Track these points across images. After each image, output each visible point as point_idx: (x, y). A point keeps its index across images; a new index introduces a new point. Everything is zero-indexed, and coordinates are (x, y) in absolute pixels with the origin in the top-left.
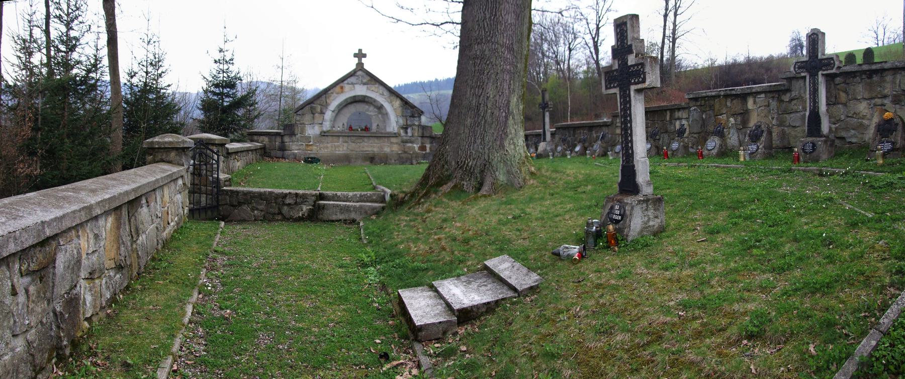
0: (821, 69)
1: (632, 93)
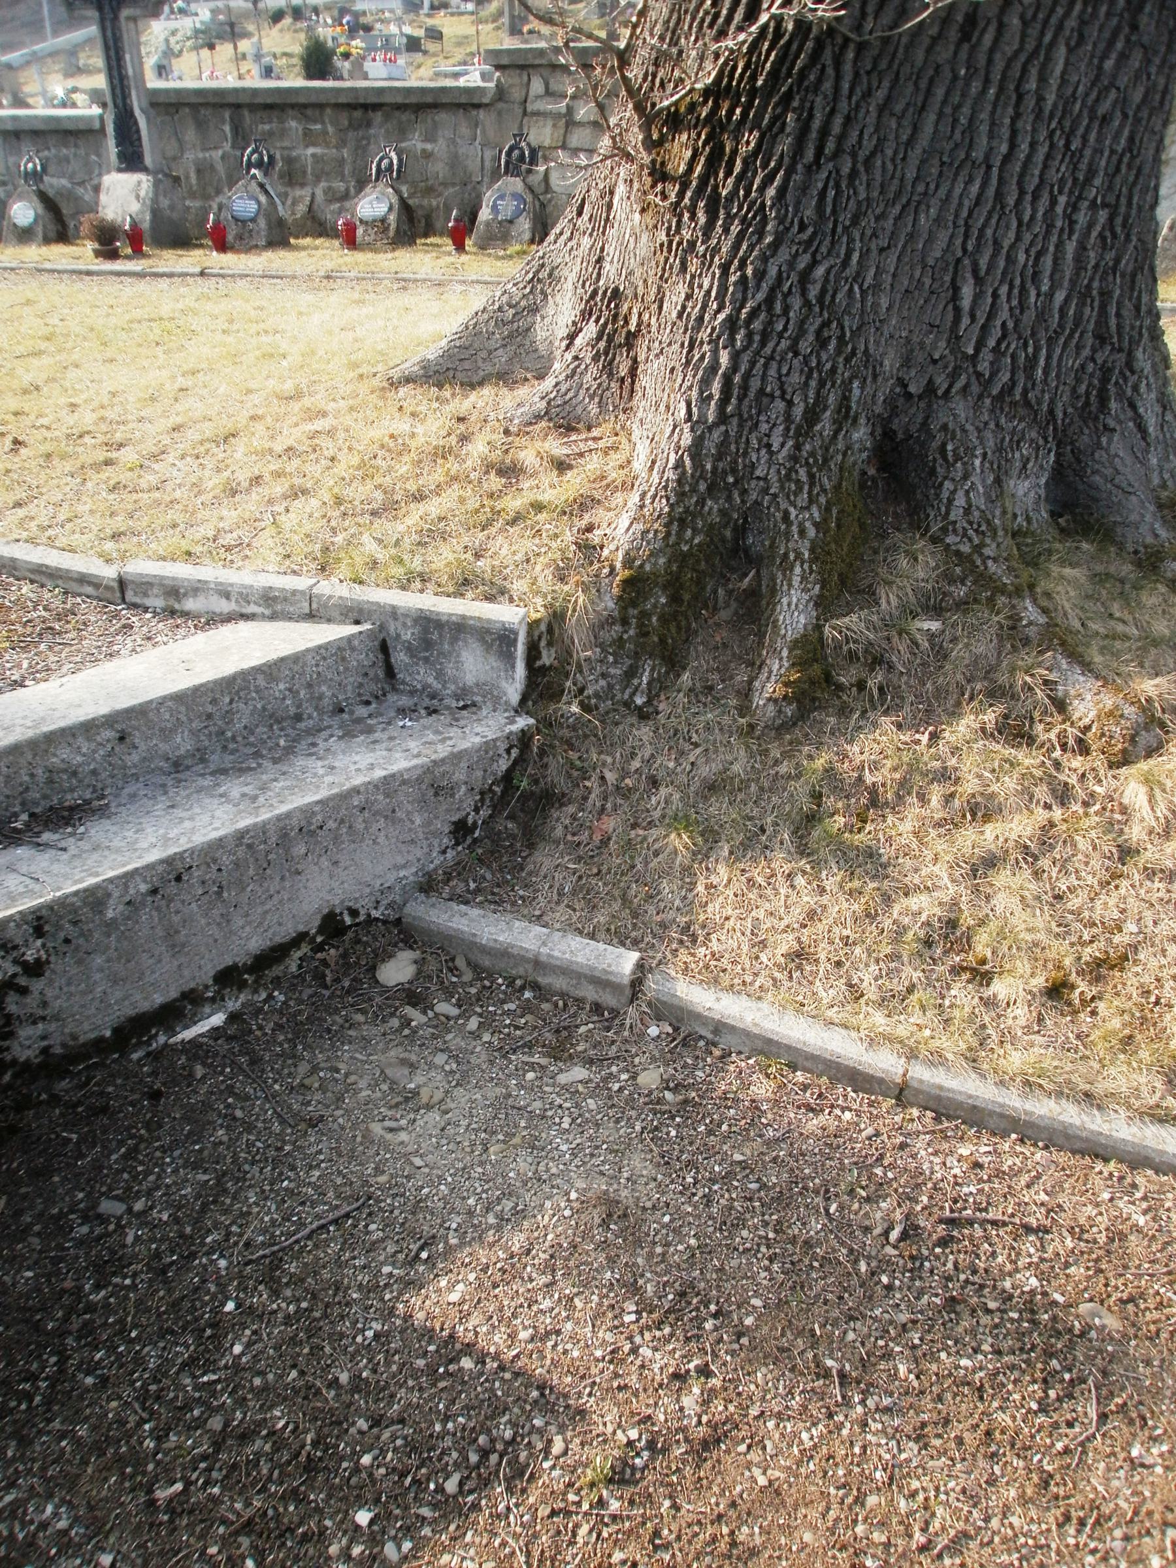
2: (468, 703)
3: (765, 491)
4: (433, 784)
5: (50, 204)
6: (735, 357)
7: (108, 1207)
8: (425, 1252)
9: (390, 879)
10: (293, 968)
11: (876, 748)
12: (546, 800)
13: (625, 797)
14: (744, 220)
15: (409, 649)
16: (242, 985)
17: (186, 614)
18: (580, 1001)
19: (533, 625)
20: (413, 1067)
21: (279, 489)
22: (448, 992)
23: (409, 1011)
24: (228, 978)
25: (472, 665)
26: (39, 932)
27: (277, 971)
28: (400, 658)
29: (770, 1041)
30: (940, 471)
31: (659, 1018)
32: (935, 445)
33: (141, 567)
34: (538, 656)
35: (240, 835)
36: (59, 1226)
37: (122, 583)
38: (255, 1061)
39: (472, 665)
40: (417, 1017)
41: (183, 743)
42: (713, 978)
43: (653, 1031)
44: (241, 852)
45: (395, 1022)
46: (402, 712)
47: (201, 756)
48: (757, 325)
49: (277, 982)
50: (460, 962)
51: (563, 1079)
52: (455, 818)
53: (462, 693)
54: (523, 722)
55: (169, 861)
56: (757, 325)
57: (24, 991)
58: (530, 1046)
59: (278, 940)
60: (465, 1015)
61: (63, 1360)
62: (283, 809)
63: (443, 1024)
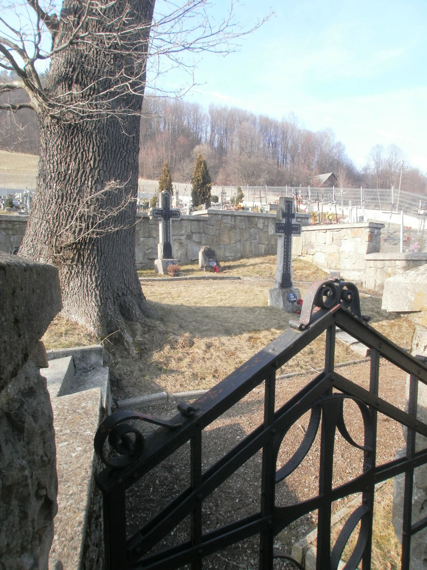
0: (171, 217)
1: (171, 223)
3: (112, 317)
6: (99, 291)
11: (156, 356)
14: (91, 266)
30: (131, 309)
32: (128, 304)
48: (101, 285)
56: (101, 285)
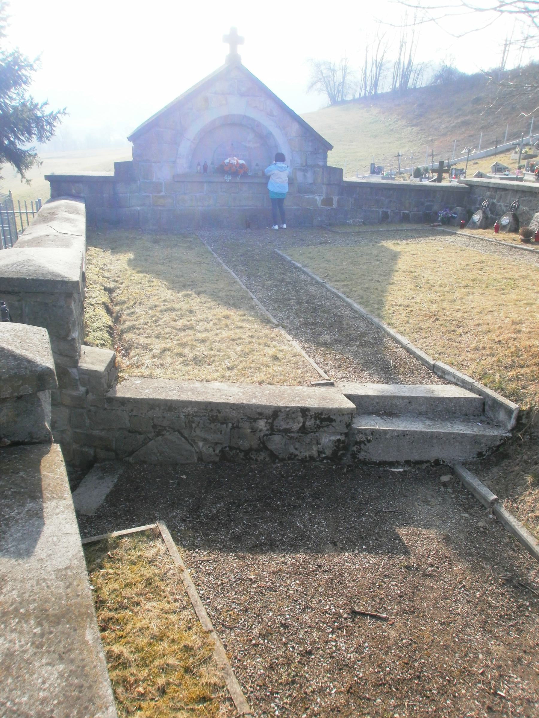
2: (498, 425)
4: (475, 440)
5: (515, 218)
7: (360, 490)
8: (406, 523)
9: (456, 458)
10: (424, 468)
12: (505, 456)
13: (526, 464)
15: (489, 406)
16: (410, 466)
17: (445, 379)
18: (480, 503)
19: (520, 411)
20: (433, 497)
21: (488, 353)
22: (453, 487)
23: (442, 487)
24: (408, 462)
25: (502, 416)
26: (372, 434)
27: (420, 466)
28: (487, 408)
29: (515, 532)
31: (494, 513)
33: (440, 364)
34: (521, 420)
35: (421, 432)
36: (350, 489)
37: (434, 366)
38: (403, 481)
39: (502, 416)
40: (442, 489)
41: (423, 409)
42: (512, 511)
43: (491, 516)
44: (420, 436)
45: (437, 488)
46: (482, 422)
47: (427, 413)
49: (419, 469)
50: (461, 483)
51: (462, 515)
52: (480, 451)
53: (498, 422)
54: (508, 434)
55: (403, 431)
57: (365, 445)
58: (461, 505)
59: (423, 459)
60: (453, 494)
61: (338, 506)
62: (434, 430)
63: (446, 493)
